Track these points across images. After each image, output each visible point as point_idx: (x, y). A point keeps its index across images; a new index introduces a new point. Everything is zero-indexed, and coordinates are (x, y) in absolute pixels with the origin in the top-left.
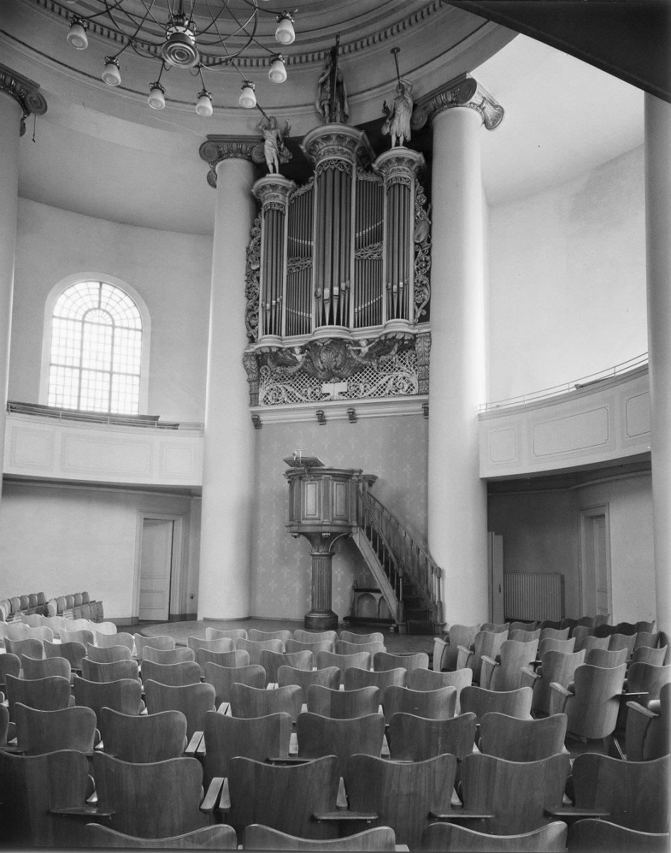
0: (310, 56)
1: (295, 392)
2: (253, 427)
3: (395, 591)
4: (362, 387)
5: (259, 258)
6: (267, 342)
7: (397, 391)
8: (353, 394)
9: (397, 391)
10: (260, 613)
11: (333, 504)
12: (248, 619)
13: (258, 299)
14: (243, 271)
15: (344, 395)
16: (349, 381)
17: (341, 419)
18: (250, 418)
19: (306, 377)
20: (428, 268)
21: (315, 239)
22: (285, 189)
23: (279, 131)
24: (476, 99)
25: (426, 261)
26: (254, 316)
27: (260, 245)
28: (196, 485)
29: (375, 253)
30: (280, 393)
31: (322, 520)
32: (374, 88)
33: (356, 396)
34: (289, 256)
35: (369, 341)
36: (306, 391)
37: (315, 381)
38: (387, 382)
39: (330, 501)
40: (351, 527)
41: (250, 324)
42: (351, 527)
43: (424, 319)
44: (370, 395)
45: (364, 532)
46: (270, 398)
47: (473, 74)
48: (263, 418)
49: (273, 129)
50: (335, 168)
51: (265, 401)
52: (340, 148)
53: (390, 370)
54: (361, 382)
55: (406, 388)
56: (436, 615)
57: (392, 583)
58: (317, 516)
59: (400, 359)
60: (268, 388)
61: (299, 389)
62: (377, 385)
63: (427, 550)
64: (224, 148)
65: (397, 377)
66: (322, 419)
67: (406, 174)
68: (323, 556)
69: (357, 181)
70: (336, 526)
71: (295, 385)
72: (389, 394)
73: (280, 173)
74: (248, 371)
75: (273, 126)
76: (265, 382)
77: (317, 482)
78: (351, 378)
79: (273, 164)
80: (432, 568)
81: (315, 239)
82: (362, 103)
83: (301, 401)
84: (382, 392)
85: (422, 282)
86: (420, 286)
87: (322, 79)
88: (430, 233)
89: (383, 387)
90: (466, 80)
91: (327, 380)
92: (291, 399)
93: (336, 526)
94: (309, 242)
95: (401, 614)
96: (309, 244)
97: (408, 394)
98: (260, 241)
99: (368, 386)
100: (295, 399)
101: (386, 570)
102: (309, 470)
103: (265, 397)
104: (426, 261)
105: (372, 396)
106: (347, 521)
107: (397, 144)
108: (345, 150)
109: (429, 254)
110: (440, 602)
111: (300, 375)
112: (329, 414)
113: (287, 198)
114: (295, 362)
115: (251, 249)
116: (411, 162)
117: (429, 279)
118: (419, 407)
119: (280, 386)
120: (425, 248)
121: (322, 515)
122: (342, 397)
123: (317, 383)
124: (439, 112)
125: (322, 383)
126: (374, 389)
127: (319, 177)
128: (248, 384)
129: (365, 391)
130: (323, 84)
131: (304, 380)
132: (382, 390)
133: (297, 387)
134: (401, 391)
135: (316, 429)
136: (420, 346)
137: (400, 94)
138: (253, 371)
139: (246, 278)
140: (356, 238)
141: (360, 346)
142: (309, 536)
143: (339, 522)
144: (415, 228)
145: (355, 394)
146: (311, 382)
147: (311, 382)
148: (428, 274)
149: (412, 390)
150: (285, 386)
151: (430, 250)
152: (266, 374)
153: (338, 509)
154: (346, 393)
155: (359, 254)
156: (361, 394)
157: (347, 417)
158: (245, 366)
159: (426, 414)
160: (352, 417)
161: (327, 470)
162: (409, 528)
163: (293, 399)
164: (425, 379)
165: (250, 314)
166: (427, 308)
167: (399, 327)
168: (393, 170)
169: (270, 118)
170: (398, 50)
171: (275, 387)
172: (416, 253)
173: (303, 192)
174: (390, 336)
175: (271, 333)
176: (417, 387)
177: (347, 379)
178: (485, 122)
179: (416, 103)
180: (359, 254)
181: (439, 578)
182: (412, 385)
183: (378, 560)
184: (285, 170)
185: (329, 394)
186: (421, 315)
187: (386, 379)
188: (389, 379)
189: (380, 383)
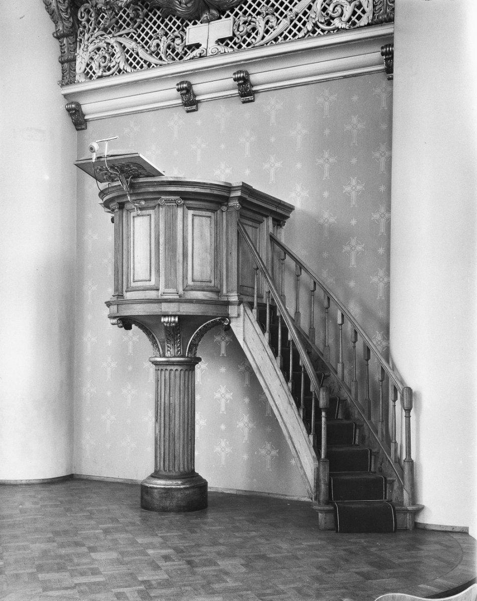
3: (311, 437)
4: (260, 23)
7: (329, 24)
8: (244, 41)
9: (329, 24)
10: (90, 468)
11: (185, 255)
12: (69, 479)
15: (227, 45)
17: (226, 97)
19: (158, 18)
30: (113, 55)
31: (160, 292)
33: (249, 45)
37: (174, 23)
38: (310, 8)
39: (180, 250)
40: (228, 304)
42: (228, 304)
44: (276, 39)
45: (253, 315)
46: (94, 65)
48: (89, 107)
51: (88, 73)
54: (259, 14)
55: (347, 13)
56: (401, 488)
57: (306, 420)
58: (153, 282)
60: (92, 47)
61: (147, 43)
62: (290, 15)
63: (387, 354)
66: (190, 100)
68: (169, 363)
70: (190, 301)
71: (139, 36)
72: (314, 32)
76: (86, 36)
77: (151, 212)
78: (241, 9)
80: (395, 390)
83: (149, 65)
84: (300, 30)
91: (195, 18)
92: (131, 64)
93: (190, 301)
95: (323, 487)
97: (353, 25)
99: (273, 21)
100: (138, 63)
101: (295, 393)
102: (132, 186)
103: (88, 65)
105: (280, 39)
106: (218, 292)
110: (411, 462)
111: (147, 15)
112: (202, 87)
118: (374, 55)
119: (112, 41)
121: (162, 279)
122: (222, 48)
123: (178, 27)
125: (187, 25)
126: (285, 22)
128: (56, 43)
129: (267, 32)
131: (155, 23)
132: (300, 25)
133: (143, 39)
134: (337, 23)
135: (180, 117)
142: (148, 325)
143: (199, 295)
145: (249, 40)
146: (166, 25)
147: (166, 25)
149: (359, 18)
150: (119, 39)
153: (200, 265)
154: (231, 39)
156: (259, 38)
157: (236, 91)
159: (389, 70)
160: (246, 90)
161: (171, 183)
162: (354, 309)
171: (103, 45)
181: (408, 411)
183: (280, 373)
185: (198, 46)
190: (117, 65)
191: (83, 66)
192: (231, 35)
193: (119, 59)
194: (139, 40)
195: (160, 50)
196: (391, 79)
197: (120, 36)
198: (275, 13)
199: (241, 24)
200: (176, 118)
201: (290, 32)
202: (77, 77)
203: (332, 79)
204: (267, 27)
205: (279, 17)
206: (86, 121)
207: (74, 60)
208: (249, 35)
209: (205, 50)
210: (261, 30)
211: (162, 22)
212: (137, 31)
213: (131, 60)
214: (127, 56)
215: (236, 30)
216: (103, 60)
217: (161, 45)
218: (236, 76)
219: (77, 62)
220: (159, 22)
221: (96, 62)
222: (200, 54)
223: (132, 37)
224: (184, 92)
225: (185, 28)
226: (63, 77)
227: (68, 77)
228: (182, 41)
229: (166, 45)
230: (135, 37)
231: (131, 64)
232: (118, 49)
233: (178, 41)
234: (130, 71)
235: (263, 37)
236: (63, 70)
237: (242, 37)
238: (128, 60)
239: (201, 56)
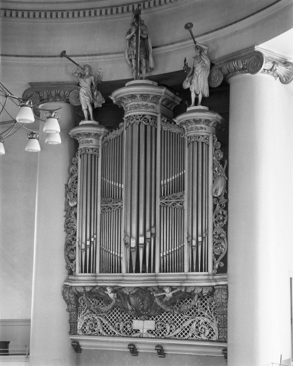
0: (93, 11)
1: (109, 325)
2: (73, 351)
4: (168, 328)
5: (77, 195)
6: (83, 281)
9: (199, 335)
13: (75, 235)
14: (63, 207)
15: (152, 333)
16: (157, 319)
18: (70, 345)
19: (119, 311)
20: (225, 222)
21: (124, 182)
22: (97, 135)
23: (92, 78)
24: (266, 65)
25: (224, 216)
26: (72, 250)
27: (77, 182)
28: (59, 135)
29: (178, 202)
32: (177, 42)
34: (102, 196)
35: (172, 288)
36: (119, 325)
38: (190, 325)
41: (69, 257)
43: (223, 270)
47: (259, 48)
49: (88, 77)
50: (140, 122)
51: (83, 330)
52: (145, 103)
53: (193, 313)
59: (201, 304)
60: (85, 318)
64: (44, 95)
65: (199, 321)
67: (204, 132)
69: (161, 131)
71: (109, 318)
73: (95, 119)
74: (68, 302)
75: (87, 74)
76: (83, 312)
78: (159, 317)
79: (88, 110)
81: (124, 182)
82: (168, 54)
85: (219, 235)
86: (218, 239)
87: (129, 36)
88: (227, 187)
89: (187, 330)
90: (255, 51)
92: (105, 331)
94: (120, 185)
96: (120, 186)
97: (209, 340)
98: (77, 179)
99: (174, 327)
103: (83, 326)
104: (224, 216)
107: (196, 104)
108: (150, 104)
109: (226, 208)
112: (141, 348)
113: (100, 141)
114: (109, 301)
115: (70, 187)
116: (207, 122)
117: (227, 233)
118: (220, 351)
119: (96, 318)
120: (222, 204)
122: (150, 335)
124: (232, 76)
126: (179, 330)
127: (127, 128)
128: (68, 313)
129: (171, 331)
130: (131, 39)
131: (117, 313)
135: (129, 357)
136: (219, 296)
137: (198, 54)
138: (72, 302)
139: (64, 213)
140: (161, 185)
141: (164, 291)
144: (213, 182)
146: (123, 316)
147: (123, 316)
148: (225, 228)
149: (212, 335)
151: (227, 204)
152: (84, 304)
154: (154, 331)
155: (163, 201)
158: (64, 298)
159: (226, 357)
163: (107, 331)
164: (223, 325)
165: (68, 249)
166: (225, 260)
167: (199, 280)
168: (192, 129)
169: (85, 66)
170: (192, 25)
171: (91, 318)
172: (215, 206)
173: (114, 137)
174: (189, 290)
175: (85, 272)
176: (217, 333)
177: (155, 317)
178: (281, 80)
179: (213, 62)
180: (163, 201)
182: (212, 331)
184: (97, 113)
186: (219, 266)
187: (189, 322)
188: (192, 322)
189: (184, 325)
190: (98, 330)
191: (81, 326)
192: (154, 329)
193: (99, 327)
194: (109, 320)
195: (120, 327)
196: (227, 361)
197: (100, 316)
198: (175, 323)
199: (159, 325)
200: (127, 356)
201: (182, 334)
202: (78, 332)
203: (188, 219)
204: (171, 329)
205: (176, 325)
206: (81, 349)
207: (77, 323)
208: (163, 331)
209: (142, 335)
210: (168, 331)
211: (121, 313)
212: (108, 315)
213: (105, 329)
214: (104, 326)
215: (156, 327)
216: (91, 326)
217: (121, 326)
218: (157, 348)
219: (78, 324)
220: (119, 313)
221: (88, 326)
222: (140, 336)
223: (106, 317)
224: (132, 349)
225: (132, 319)
226: (71, 329)
227: (73, 330)
228: (131, 326)
229: (123, 326)
230: (108, 318)
231: (105, 331)
232: (99, 323)
233: (128, 326)
234: (105, 335)
235: (169, 333)
236: (70, 326)
237: (159, 331)
238: (104, 328)
239: (140, 337)
